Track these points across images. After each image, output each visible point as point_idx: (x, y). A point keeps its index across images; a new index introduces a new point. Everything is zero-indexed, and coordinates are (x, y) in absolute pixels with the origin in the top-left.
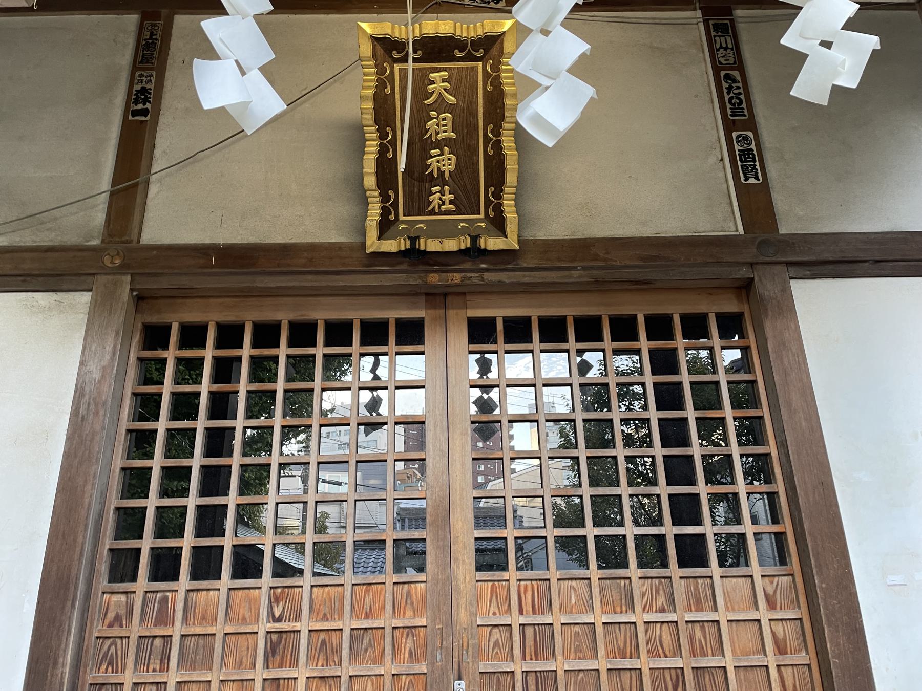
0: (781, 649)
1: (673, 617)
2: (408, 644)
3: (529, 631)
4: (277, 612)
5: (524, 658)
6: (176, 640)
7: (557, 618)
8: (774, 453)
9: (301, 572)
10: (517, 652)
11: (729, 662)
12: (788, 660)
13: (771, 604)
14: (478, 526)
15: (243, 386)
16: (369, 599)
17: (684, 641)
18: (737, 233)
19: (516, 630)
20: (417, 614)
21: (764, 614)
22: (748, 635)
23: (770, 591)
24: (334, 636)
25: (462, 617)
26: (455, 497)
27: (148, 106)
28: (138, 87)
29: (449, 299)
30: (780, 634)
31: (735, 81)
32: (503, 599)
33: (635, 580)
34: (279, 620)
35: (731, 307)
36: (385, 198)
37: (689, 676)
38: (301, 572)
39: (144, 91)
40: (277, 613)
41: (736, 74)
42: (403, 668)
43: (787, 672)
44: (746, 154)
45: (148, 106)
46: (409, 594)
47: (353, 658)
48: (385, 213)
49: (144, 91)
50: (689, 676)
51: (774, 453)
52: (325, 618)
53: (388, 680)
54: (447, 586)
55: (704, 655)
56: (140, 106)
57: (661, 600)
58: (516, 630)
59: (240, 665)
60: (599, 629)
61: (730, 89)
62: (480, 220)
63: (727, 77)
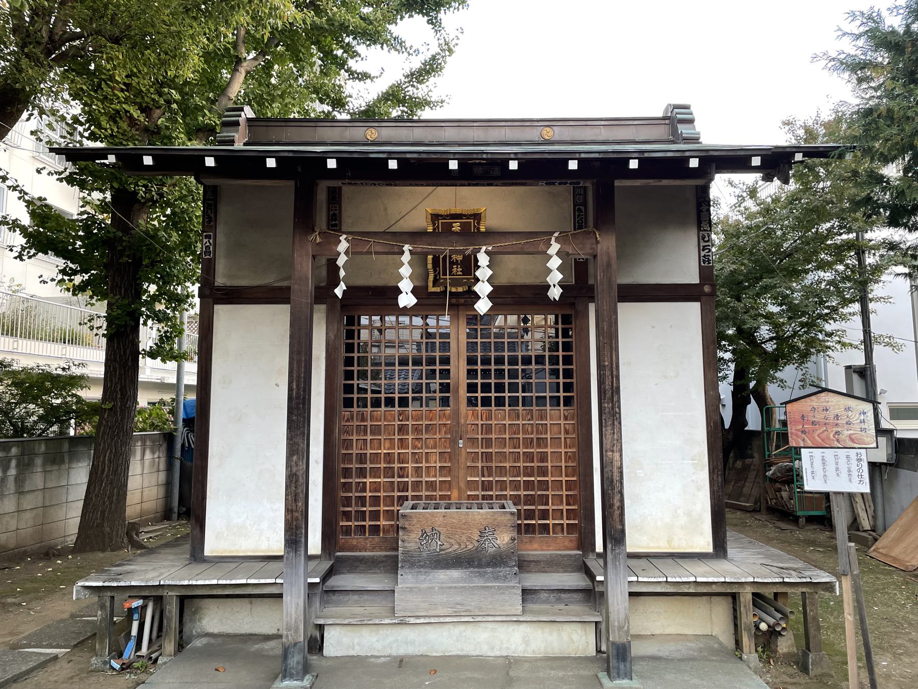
0: (567, 432)
1: (532, 422)
2: (444, 430)
3: (484, 426)
4: (401, 418)
5: (482, 434)
6: (369, 426)
7: (493, 422)
8: (575, 369)
9: (366, 390)
10: (480, 432)
11: (549, 436)
12: (568, 436)
13: (566, 418)
14: (468, 392)
15: (522, 493)
16: (431, 415)
17: (535, 429)
18: (313, 617)
19: (480, 425)
20: (447, 420)
21: (562, 422)
22: (556, 429)
23: (566, 414)
24: (420, 427)
25: (462, 421)
26: (461, 382)
27: (337, 222)
28: (331, 213)
29: (460, 307)
30: (567, 428)
31: (581, 212)
32: (476, 416)
33: (520, 411)
34: (401, 421)
35: (567, 312)
36: (435, 271)
37: (535, 440)
38: (366, 390)
39: (334, 215)
40: (401, 418)
41: (582, 208)
42: (443, 436)
43: (568, 440)
44: (373, 562)
45: (337, 222)
46: (444, 414)
47: (426, 433)
48: (435, 276)
49: (334, 215)
50: (535, 440)
51: (575, 369)
52: (416, 421)
53: (438, 440)
54: (456, 414)
55: (541, 434)
56: (334, 222)
57: (529, 417)
58: (480, 425)
59: (389, 434)
60: (507, 426)
61: (579, 216)
62: (472, 278)
63: (579, 209)
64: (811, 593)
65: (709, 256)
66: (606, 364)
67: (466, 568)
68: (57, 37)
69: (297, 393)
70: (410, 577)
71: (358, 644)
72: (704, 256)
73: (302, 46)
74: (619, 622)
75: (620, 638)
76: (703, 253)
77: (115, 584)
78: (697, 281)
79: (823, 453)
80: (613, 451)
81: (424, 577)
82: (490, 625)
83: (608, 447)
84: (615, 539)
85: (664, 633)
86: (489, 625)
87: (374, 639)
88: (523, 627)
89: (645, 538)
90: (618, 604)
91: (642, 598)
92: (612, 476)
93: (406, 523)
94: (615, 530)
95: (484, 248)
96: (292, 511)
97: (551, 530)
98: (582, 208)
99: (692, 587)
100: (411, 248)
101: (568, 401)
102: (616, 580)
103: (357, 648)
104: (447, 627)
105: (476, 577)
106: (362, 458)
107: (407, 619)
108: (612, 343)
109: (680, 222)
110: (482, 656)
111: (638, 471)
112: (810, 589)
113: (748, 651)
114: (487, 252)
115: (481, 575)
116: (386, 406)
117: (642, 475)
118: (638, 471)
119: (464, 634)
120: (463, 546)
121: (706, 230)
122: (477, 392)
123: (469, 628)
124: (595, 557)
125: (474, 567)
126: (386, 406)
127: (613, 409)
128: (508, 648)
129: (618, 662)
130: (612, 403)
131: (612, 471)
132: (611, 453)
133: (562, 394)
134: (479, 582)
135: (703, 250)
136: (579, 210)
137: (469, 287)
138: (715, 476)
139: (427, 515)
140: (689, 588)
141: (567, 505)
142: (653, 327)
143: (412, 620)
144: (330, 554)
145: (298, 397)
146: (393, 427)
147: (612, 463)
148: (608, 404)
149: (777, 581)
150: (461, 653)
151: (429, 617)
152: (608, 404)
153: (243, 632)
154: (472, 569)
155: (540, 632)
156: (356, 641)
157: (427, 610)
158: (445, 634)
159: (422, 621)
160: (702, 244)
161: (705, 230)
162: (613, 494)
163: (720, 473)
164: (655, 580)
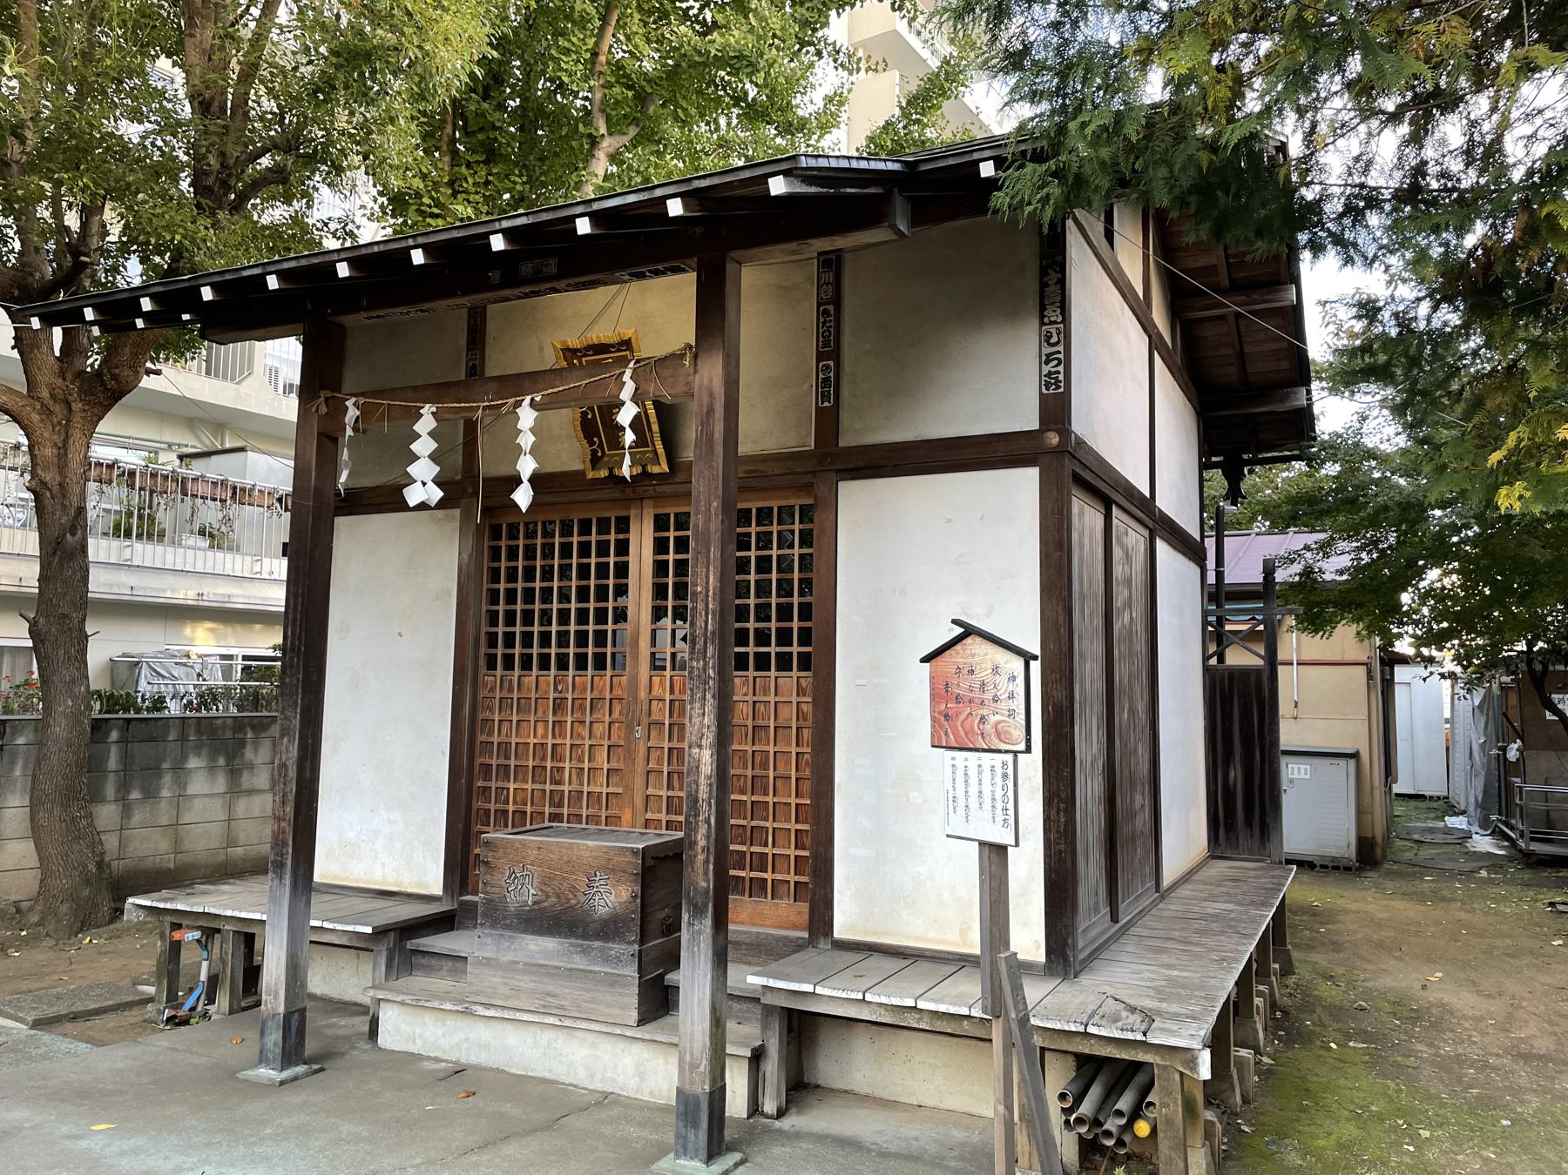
29: (645, 501)
31: (829, 315)
49: (474, 366)
61: (824, 323)
64: (1165, 1068)
65: (1059, 372)
66: (699, 589)
67: (567, 937)
68: (232, 161)
69: (292, 644)
70: (489, 941)
71: (420, 1037)
72: (1049, 375)
73: (684, 97)
74: (692, 1055)
75: (692, 1083)
76: (1046, 369)
77: (169, 906)
78: (1035, 426)
79: (953, 759)
80: (700, 747)
81: (507, 944)
82: (590, 1037)
83: (694, 738)
84: (695, 906)
85: (941, 1106)
86: (587, 1035)
87: (440, 1033)
88: (637, 1048)
89: (920, 922)
90: (692, 1023)
91: (906, 1032)
92: (697, 791)
93: (491, 854)
94: (696, 890)
95: (528, 399)
96: (279, 820)
97: (769, 891)
98: (831, 308)
99: (926, 1019)
100: (434, 409)
101: (805, 662)
102: (693, 979)
103: (418, 1041)
104: (532, 1029)
105: (577, 953)
106: (504, 748)
107: (474, 1007)
108: (709, 551)
109: (1009, 313)
110: (576, 1086)
111: (911, 794)
112: (1163, 1058)
113: (1027, 1166)
114: (533, 404)
115: (584, 951)
116: (757, 669)
117: (920, 801)
118: (911, 794)
119: (554, 1045)
120: (563, 900)
121: (1055, 322)
122: (770, 645)
123: (561, 1034)
124: (829, 947)
125: (577, 937)
126: (778, 669)
127: (705, 669)
128: (614, 1080)
129: (686, 1127)
130: (704, 660)
131: (697, 783)
132: (697, 750)
133: (795, 649)
134: (579, 962)
135: (1047, 363)
136: (826, 312)
137: (611, 470)
138: (1053, 812)
139: (517, 845)
140: (920, 1020)
141: (797, 847)
142: (950, 520)
143: (480, 1010)
144: (453, 897)
145: (292, 650)
146: (779, 705)
147: (698, 767)
148: (698, 661)
149: (1073, 1029)
150: (548, 1075)
151: (503, 1008)
152: (698, 661)
153: (347, 998)
154: (573, 941)
155: (661, 1061)
156: (418, 1030)
157: (507, 998)
158: (529, 1040)
159: (491, 1013)
160: (1047, 350)
161: (1051, 323)
162: (697, 823)
163: (1062, 806)
164: (844, 995)
